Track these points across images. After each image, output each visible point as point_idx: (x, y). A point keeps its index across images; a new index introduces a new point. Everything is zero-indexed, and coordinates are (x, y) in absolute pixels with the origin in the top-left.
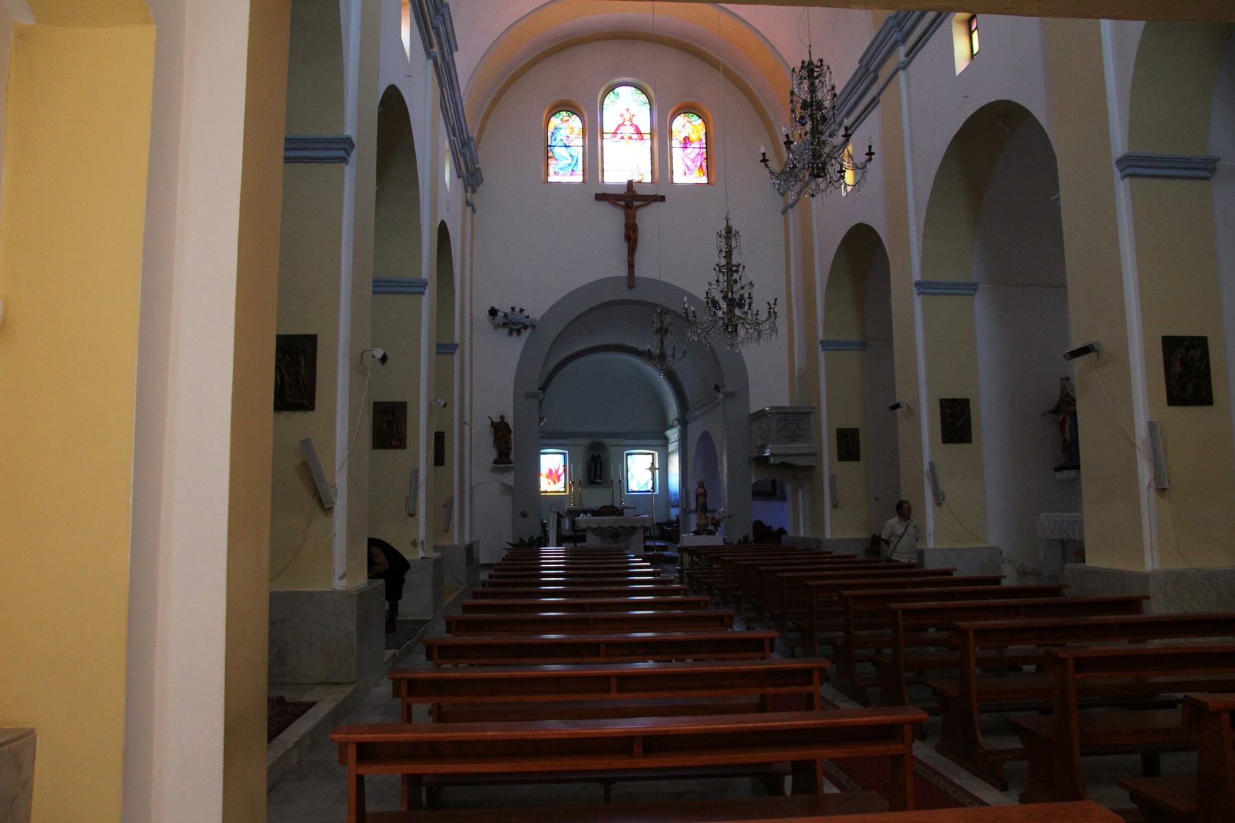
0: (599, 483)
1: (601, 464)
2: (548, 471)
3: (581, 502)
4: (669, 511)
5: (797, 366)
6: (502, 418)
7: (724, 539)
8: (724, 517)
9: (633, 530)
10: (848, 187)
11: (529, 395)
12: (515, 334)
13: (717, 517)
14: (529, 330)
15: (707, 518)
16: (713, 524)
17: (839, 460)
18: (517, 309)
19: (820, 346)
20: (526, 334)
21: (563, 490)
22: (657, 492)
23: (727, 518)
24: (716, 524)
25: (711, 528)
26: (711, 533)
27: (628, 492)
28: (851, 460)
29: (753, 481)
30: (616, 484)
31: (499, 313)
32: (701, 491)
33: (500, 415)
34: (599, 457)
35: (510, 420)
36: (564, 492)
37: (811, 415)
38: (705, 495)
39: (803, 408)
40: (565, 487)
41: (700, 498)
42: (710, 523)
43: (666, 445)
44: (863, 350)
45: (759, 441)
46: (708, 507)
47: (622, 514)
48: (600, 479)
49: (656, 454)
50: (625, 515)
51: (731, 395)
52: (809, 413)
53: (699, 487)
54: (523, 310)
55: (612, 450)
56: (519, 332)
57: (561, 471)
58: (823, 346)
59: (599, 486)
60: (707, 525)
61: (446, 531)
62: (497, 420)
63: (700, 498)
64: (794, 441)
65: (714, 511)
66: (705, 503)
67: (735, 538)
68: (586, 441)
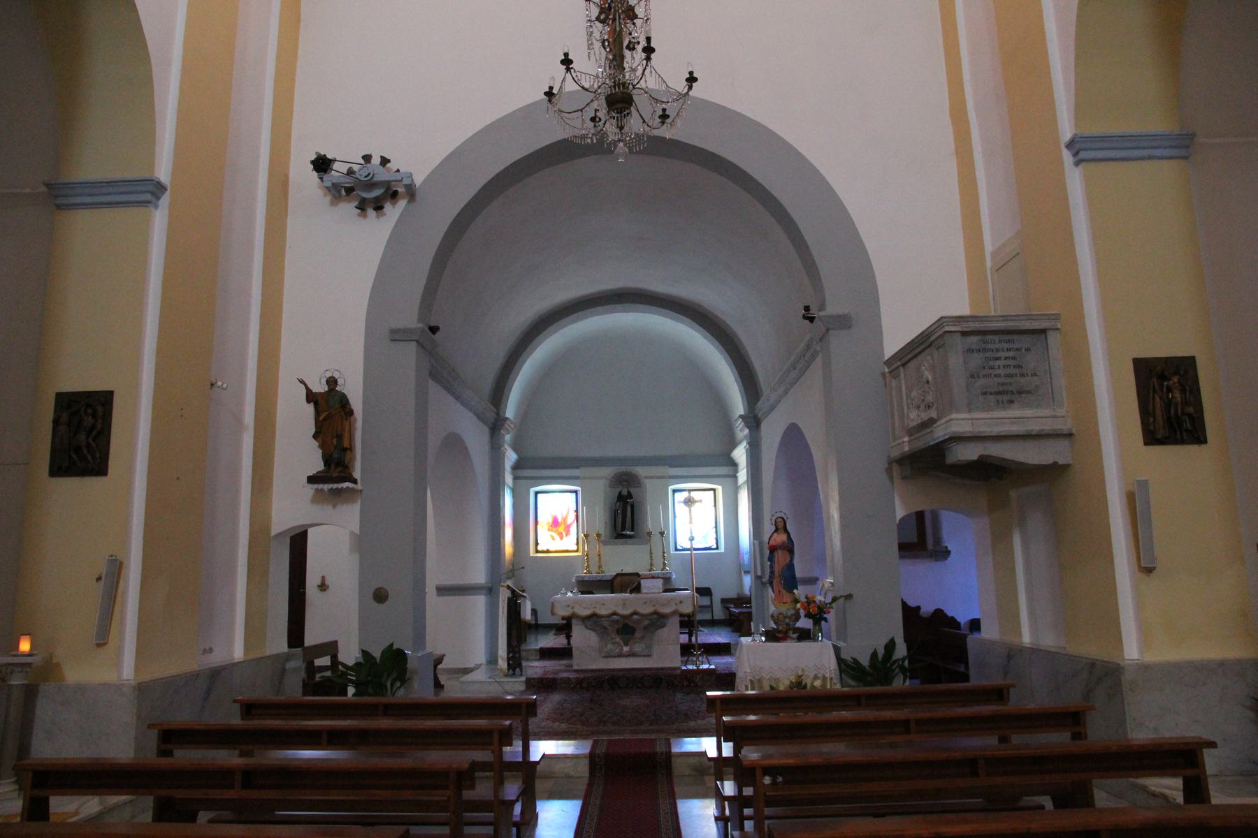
0: (630, 537)
1: (632, 506)
2: (550, 520)
3: (600, 567)
4: (740, 577)
5: (989, 247)
6: (332, 382)
7: (837, 650)
8: (834, 599)
9: (657, 620)
10: (746, 822)
11: (398, 335)
12: (371, 213)
13: (819, 598)
14: (402, 204)
15: (796, 601)
16: (808, 615)
17: (1146, 444)
18: (376, 160)
19: (1067, 157)
20: (393, 211)
21: (575, 548)
22: (722, 549)
23: (842, 600)
24: (818, 615)
25: (804, 623)
26: (804, 635)
27: (676, 549)
28: (1182, 442)
29: (900, 513)
30: (656, 538)
31: (336, 166)
32: (780, 538)
33: (329, 375)
34: (630, 495)
35: (354, 390)
36: (577, 551)
37: (1052, 337)
38: (789, 548)
39: (1029, 317)
40: (577, 544)
41: (781, 556)
42: (802, 612)
43: (734, 477)
44: (1186, 158)
45: (913, 415)
46: (798, 574)
47: (637, 589)
48: (632, 530)
49: (719, 489)
50: (644, 590)
51: (844, 322)
52: (1043, 331)
53: (776, 530)
54: (389, 161)
55: (649, 485)
56: (379, 208)
57: (572, 517)
58: (1075, 155)
59: (629, 541)
60: (797, 618)
61: (99, 645)
62: (319, 387)
63: (781, 556)
64: (1011, 402)
65: (812, 581)
66: (790, 567)
67: (862, 649)
68: (608, 472)
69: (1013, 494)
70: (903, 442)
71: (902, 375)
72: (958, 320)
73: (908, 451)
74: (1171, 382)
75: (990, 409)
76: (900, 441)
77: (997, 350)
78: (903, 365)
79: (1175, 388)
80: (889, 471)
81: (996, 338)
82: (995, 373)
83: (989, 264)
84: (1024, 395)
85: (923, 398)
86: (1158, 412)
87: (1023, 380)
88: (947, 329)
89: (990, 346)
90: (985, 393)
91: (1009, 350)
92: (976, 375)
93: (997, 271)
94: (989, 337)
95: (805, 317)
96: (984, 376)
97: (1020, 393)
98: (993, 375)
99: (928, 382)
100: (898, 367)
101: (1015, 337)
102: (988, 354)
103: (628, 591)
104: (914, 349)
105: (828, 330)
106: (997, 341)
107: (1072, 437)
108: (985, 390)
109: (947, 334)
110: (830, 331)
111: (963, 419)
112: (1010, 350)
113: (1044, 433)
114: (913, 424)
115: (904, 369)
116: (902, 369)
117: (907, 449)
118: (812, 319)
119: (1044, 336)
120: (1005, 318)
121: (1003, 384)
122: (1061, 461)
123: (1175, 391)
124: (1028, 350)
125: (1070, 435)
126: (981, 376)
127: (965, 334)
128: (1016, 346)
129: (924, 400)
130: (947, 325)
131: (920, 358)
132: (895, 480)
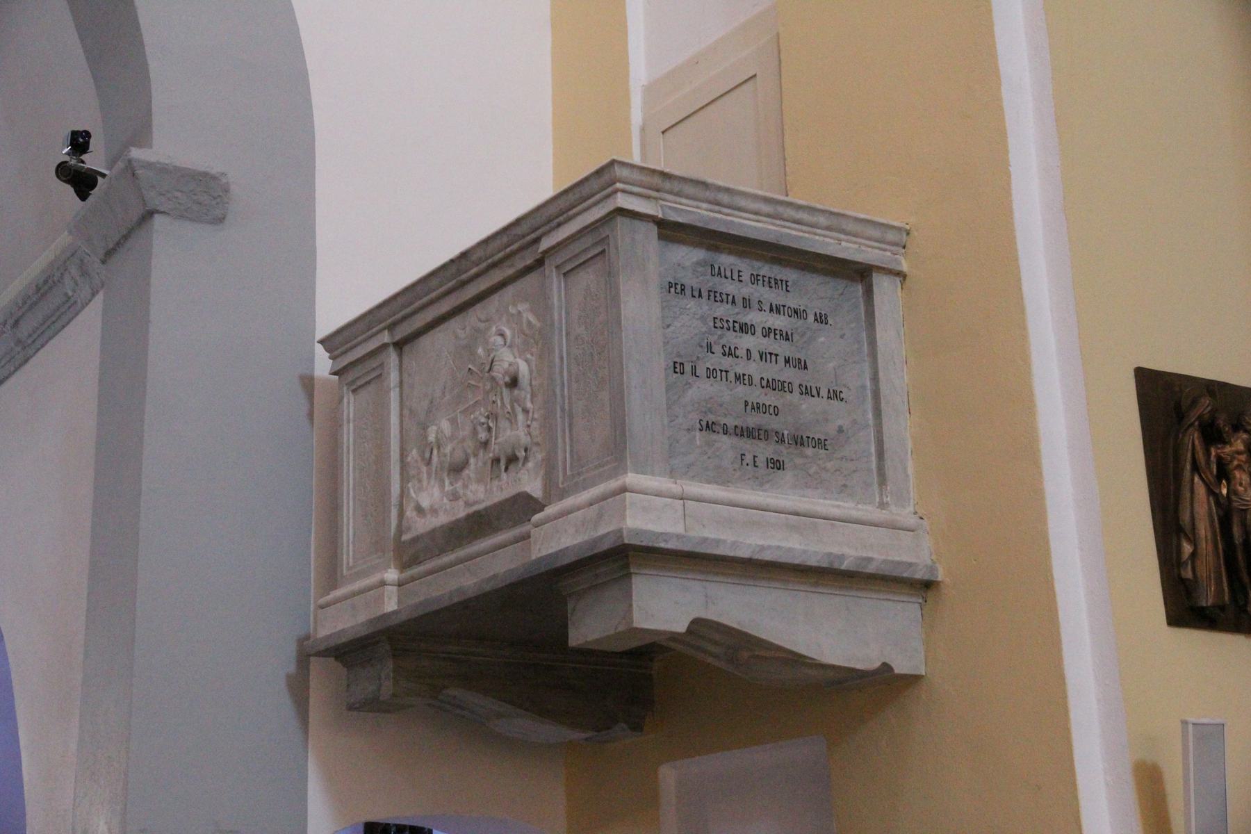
5: (640, 72)
52: (861, 273)
64: (776, 465)
69: (668, 775)
70: (383, 583)
71: (394, 377)
72: (656, 180)
73: (394, 613)
74: (1228, 449)
75: (721, 478)
76: (374, 579)
77: (746, 303)
78: (400, 345)
79: (1239, 467)
80: (299, 688)
81: (746, 267)
82: (740, 371)
83: (637, 117)
84: (809, 451)
85: (483, 435)
86: (1203, 529)
87: (809, 407)
88: (622, 201)
89: (730, 287)
90: (710, 427)
91: (776, 309)
92: (688, 368)
93: (663, 132)
94: (726, 260)
95: (66, 173)
96: (711, 373)
97: (799, 441)
98: (731, 376)
99: (514, 383)
100: (384, 347)
101: (791, 275)
102: (722, 310)
103: (312, 640)
104: (463, 284)
105: (149, 215)
106: (746, 277)
107: (930, 594)
108: (711, 418)
109: (620, 221)
110: (158, 219)
111: (658, 494)
112: (778, 311)
113: (871, 569)
114: (421, 526)
115: (400, 355)
116: (392, 357)
117: (391, 605)
118: (83, 182)
119: (859, 289)
120: (776, 207)
121: (757, 408)
122: (900, 667)
123: (1237, 474)
124: (821, 319)
125: (926, 586)
126: (701, 371)
127: (670, 231)
128: (793, 302)
129: (485, 444)
130: (624, 191)
131: (473, 317)
132: (314, 716)
